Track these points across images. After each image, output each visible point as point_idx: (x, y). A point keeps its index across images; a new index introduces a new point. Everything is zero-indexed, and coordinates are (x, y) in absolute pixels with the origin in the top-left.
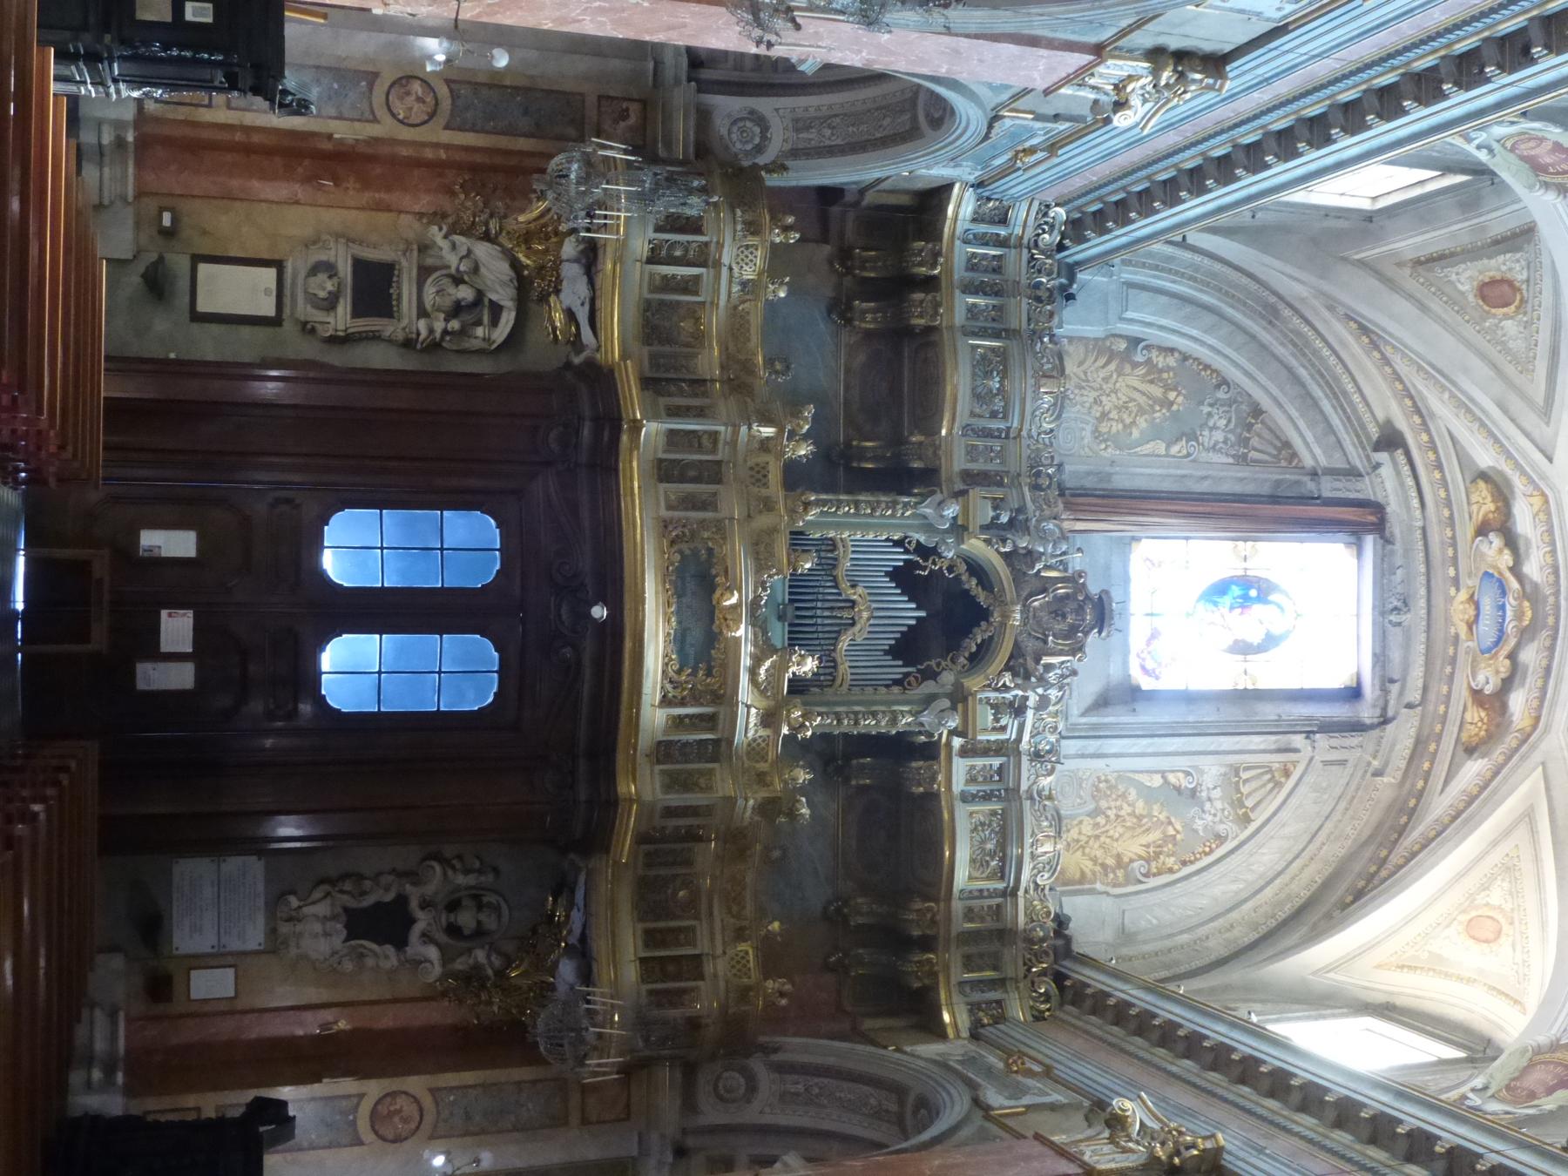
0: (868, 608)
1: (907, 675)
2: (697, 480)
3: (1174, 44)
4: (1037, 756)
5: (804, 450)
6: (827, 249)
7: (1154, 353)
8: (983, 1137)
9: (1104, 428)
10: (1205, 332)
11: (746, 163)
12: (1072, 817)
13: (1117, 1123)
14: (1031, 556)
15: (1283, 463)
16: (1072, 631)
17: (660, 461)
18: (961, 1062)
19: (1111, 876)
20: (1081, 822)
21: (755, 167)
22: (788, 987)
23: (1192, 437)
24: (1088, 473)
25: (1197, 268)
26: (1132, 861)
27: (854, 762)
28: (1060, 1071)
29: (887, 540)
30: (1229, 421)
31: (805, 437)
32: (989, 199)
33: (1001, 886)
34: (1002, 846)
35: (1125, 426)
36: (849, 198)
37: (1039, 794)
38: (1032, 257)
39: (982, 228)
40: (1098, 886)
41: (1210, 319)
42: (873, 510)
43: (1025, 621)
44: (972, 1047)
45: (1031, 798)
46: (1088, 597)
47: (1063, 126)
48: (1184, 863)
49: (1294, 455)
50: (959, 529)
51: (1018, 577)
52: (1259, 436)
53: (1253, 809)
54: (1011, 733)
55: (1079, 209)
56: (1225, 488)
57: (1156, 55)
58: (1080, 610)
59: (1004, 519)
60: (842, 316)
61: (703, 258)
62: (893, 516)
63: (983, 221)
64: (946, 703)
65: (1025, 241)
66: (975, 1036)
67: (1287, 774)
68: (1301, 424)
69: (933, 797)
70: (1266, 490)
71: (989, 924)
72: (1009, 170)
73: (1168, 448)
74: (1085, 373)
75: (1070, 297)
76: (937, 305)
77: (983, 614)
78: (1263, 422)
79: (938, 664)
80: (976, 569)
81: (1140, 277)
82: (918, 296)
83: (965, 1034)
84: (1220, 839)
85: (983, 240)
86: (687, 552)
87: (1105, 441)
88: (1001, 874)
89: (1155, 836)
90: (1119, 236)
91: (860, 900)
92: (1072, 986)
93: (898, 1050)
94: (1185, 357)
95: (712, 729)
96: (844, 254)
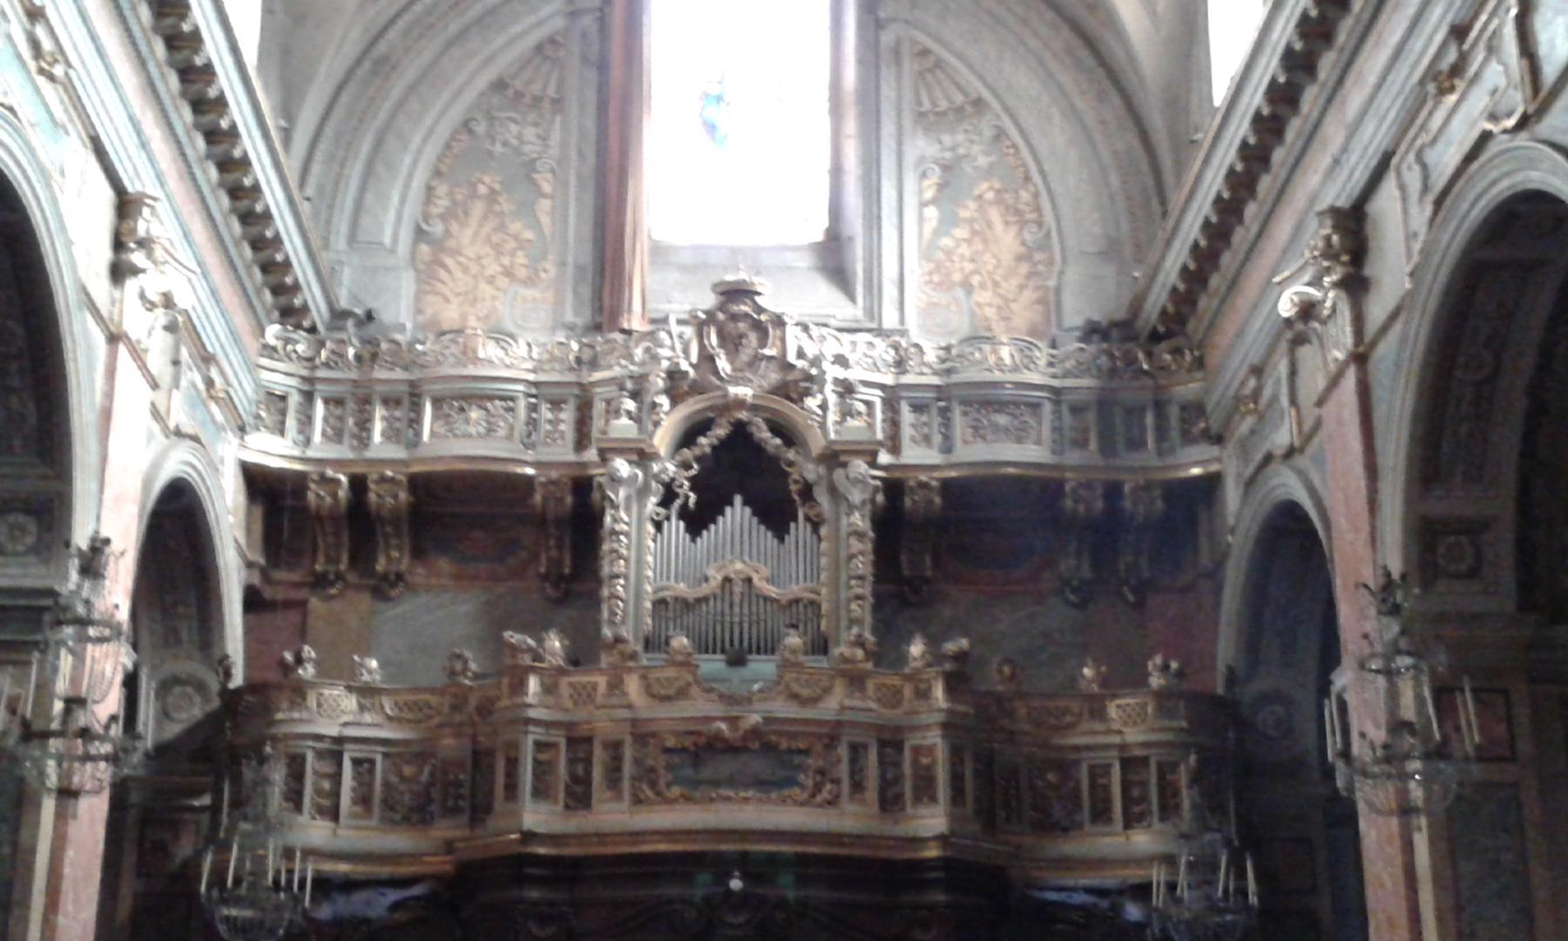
0: (732, 562)
1: (808, 519)
2: (588, 762)
3: (105, 254)
4: (900, 365)
5: (555, 643)
6: (315, 603)
7: (435, 211)
8: (1319, 461)
9: (522, 273)
10: (405, 147)
11: (216, 703)
12: (973, 315)
13: (1308, 310)
14: (674, 375)
15: (561, 53)
16: (759, 327)
17: (567, 807)
18: (1246, 462)
19: (1041, 268)
20: (978, 304)
21: (226, 694)
22: (1158, 660)
23: (530, 166)
24: (575, 292)
25: (331, 157)
26: (1024, 243)
27: (906, 573)
28: (1254, 357)
29: (654, 541)
30: (510, 119)
31: (540, 641)
32: (258, 417)
33: (1048, 408)
34: (1000, 405)
35: (521, 248)
36: (256, 580)
37: (943, 361)
38: (326, 365)
39: (291, 423)
40: (1052, 283)
41: (392, 142)
42: (621, 557)
43: (746, 382)
44: (1231, 446)
45: (949, 372)
46: (721, 308)
47: (184, 354)
48: (1027, 179)
49: (552, 41)
50: (642, 457)
51: (697, 389)
52: (530, 82)
53: (965, 93)
54: (876, 396)
55: (268, 313)
56: (590, 125)
57: (119, 272)
58: (734, 317)
59: (630, 405)
60: (393, 585)
61: (334, 750)
62: (627, 535)
63: (283, 423)
64: (839, 474)
65: (305, 373)
66: (1218, 439)
67: (925, 53)
68: (516, 29)
69: (947, 486)
70: (592, 76)
71: (1091, 417)
72: (228, 403)
73: (544, 196)
74: (458, 294)
75: (370, 316)
76: (383, 479)
77: (740, 429)
78: (514, 77)
79: (796, 482)
80: (687, 438)
81: (342, 225)
82: (372, 497)
83: (1215, 451)
84: (1000, 134)
85: (306, 421)
86: (670, 776)
87: (536, 272)
88: (1035, 406)
89: (995, 215)
90: (302, 270)
91: (1062, 567)
92: (1164, 324)
93: (1233, 531)
94: (437, 173)
95: (865, 747)
96: (320, 583)
